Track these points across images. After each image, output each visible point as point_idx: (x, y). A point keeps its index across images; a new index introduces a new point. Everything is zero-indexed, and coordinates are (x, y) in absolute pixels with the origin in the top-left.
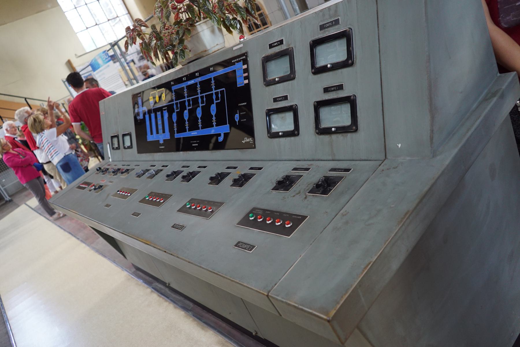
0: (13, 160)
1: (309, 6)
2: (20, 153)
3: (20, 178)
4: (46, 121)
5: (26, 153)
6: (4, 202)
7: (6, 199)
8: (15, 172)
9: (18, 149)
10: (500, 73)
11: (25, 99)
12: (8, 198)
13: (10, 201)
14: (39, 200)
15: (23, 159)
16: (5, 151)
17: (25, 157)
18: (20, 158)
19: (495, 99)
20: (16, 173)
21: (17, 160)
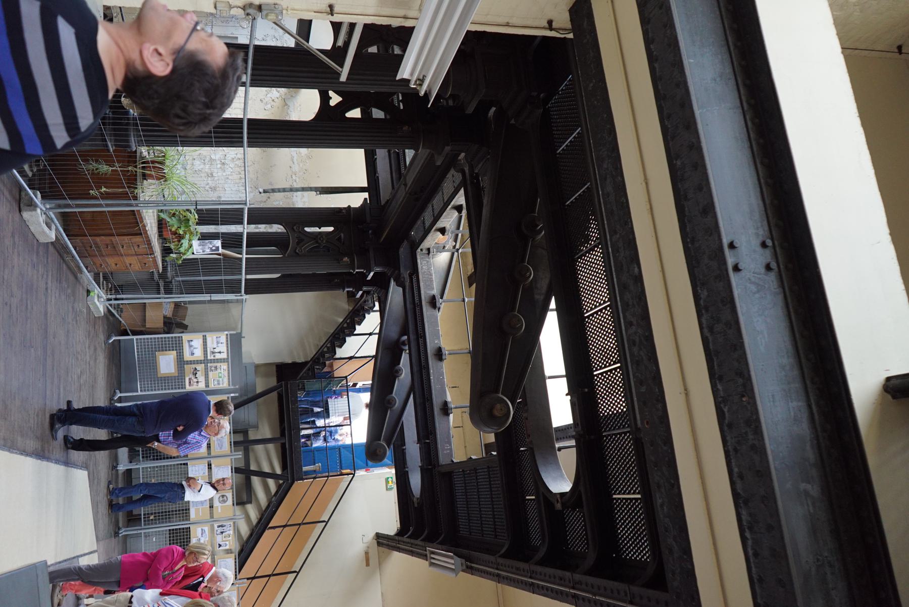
0: (167, 558)
1: (274, 368)
2: (174, 573)
3: (133, 556)
4: (219, 380)
5: (168, 583)
6: (121, 525)
7: (123, 530)
8: (148, 552)
9: (182, 574)
10: (468, 32)
11: (298, 573)
12: (123, 532)
13: (116, 534)
14: (80, 568)
15: (161, 574)
16: (187, 554)
17: (164, 579)
18: (165, 570)
19: (405, 358)
20: (145, 554)
21: (165, 563)
